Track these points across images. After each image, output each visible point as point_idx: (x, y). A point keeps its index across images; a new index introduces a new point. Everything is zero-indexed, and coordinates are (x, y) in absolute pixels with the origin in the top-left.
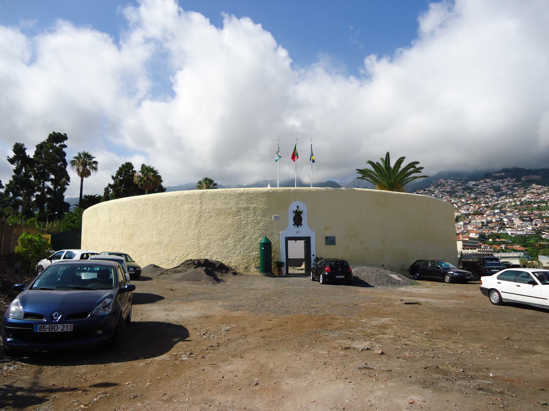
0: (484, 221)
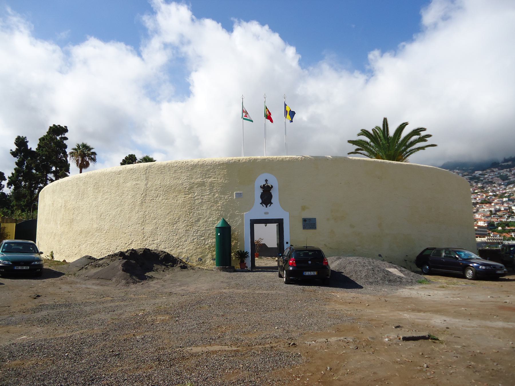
0: (492, 209)
